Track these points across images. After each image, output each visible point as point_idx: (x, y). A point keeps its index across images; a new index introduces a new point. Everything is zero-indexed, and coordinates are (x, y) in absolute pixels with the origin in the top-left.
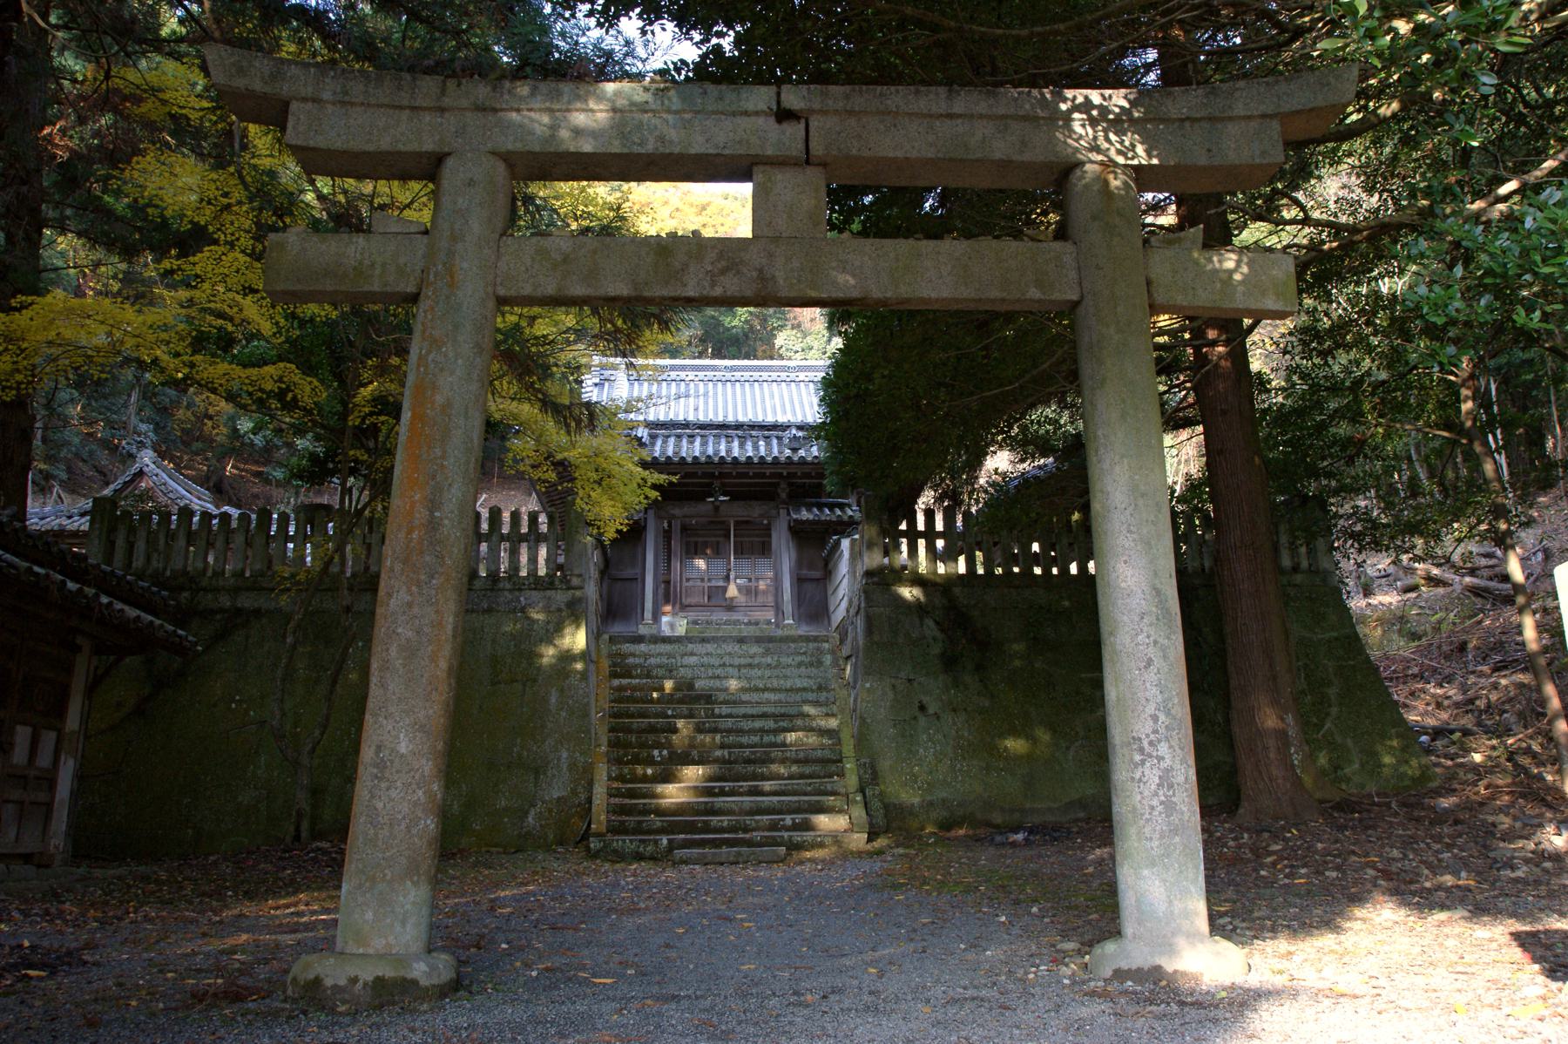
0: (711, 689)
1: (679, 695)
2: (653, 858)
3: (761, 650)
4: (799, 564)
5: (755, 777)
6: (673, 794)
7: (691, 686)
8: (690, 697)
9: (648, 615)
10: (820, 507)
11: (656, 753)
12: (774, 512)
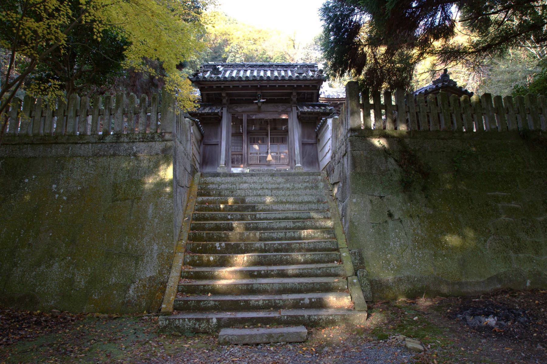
0: (255, 202)
1: (236, 206)
2: (205, 332)
3: (283, 180)
4: (303, 135)
5: (281, 262)
6: (227, 277)
7: (243, 201)
8: (243, 207)
10: (314, 106)
11: (217, 244)
12: (289, 109)
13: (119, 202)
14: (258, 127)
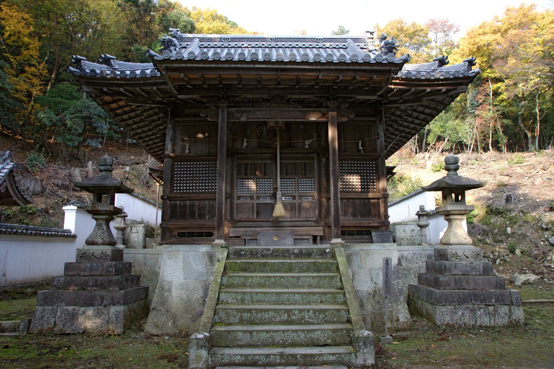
14: (254, 142)
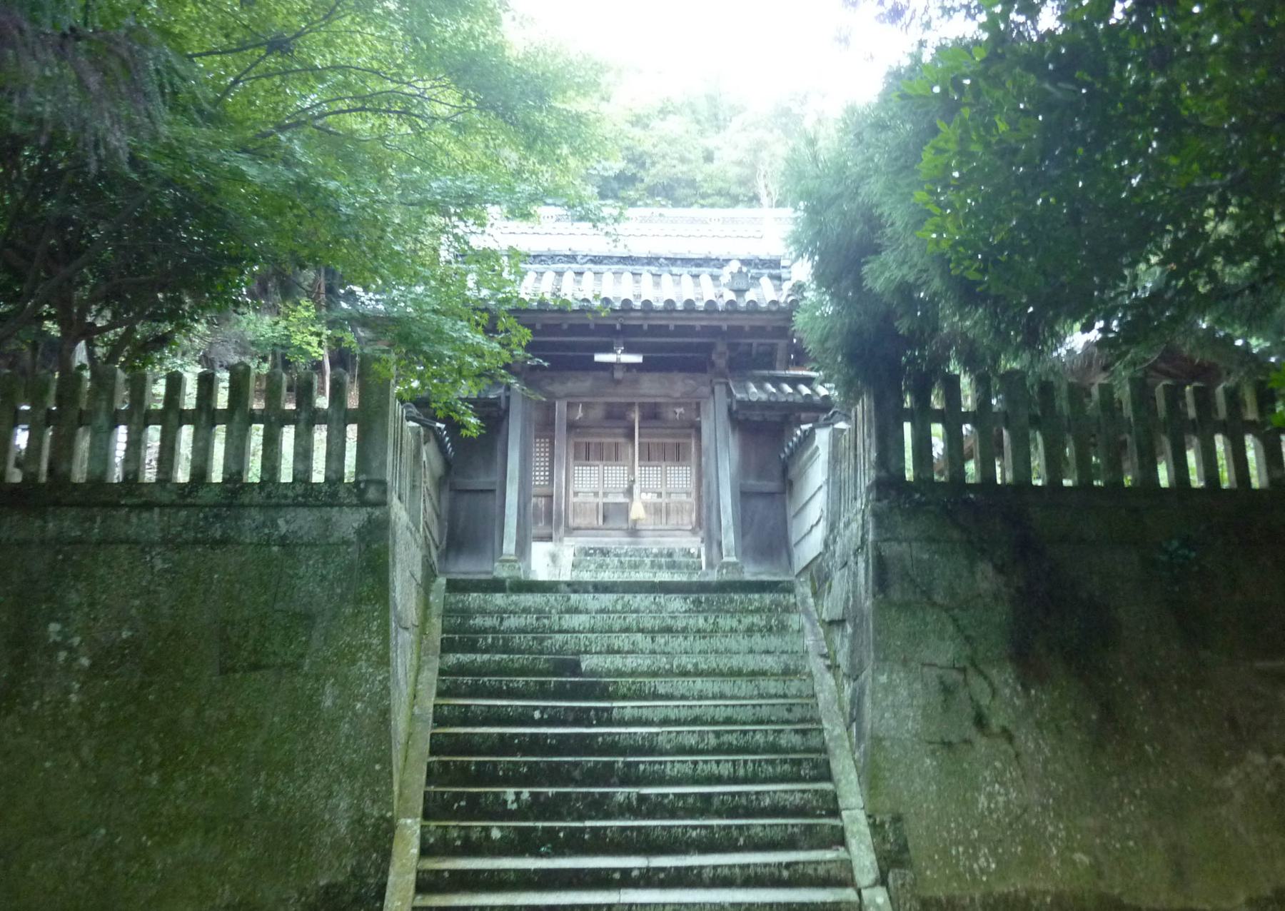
4: (744, 469)
9: (509, 547)
13: (238, 676)
